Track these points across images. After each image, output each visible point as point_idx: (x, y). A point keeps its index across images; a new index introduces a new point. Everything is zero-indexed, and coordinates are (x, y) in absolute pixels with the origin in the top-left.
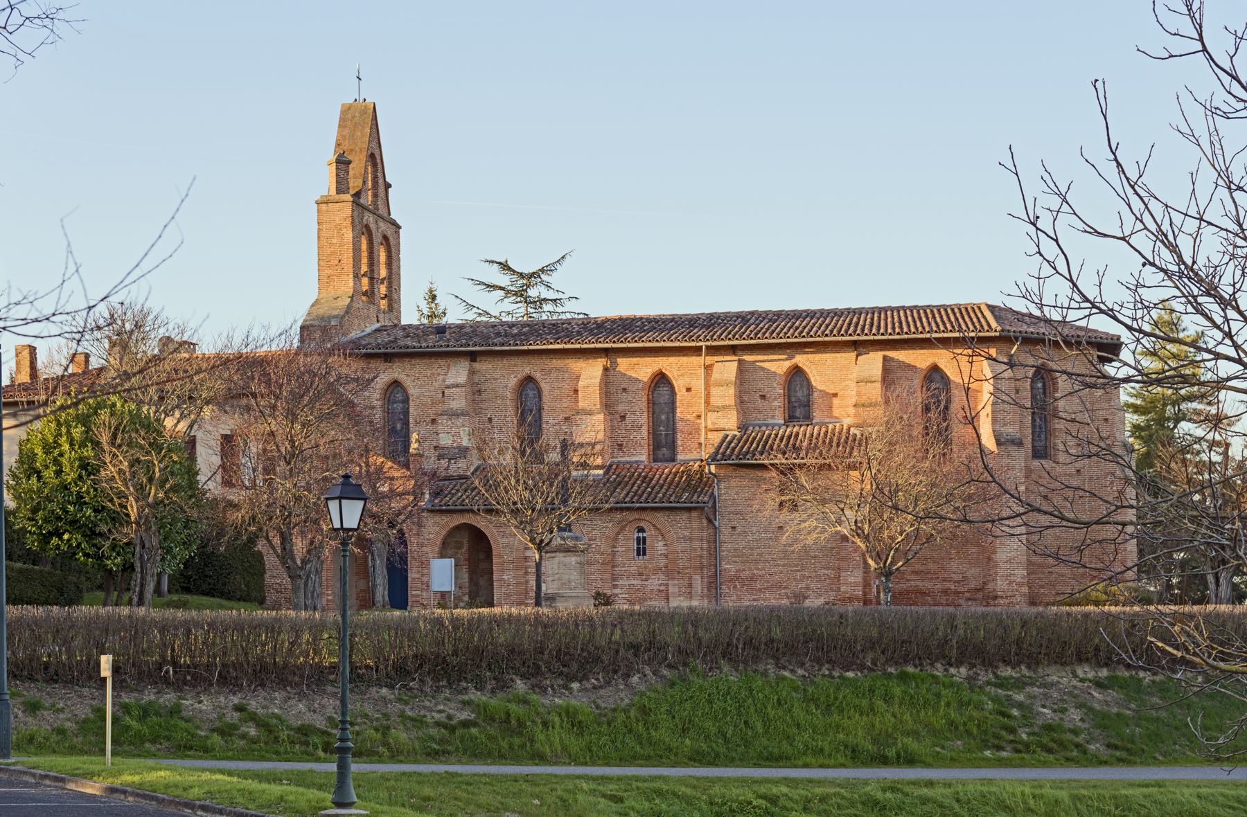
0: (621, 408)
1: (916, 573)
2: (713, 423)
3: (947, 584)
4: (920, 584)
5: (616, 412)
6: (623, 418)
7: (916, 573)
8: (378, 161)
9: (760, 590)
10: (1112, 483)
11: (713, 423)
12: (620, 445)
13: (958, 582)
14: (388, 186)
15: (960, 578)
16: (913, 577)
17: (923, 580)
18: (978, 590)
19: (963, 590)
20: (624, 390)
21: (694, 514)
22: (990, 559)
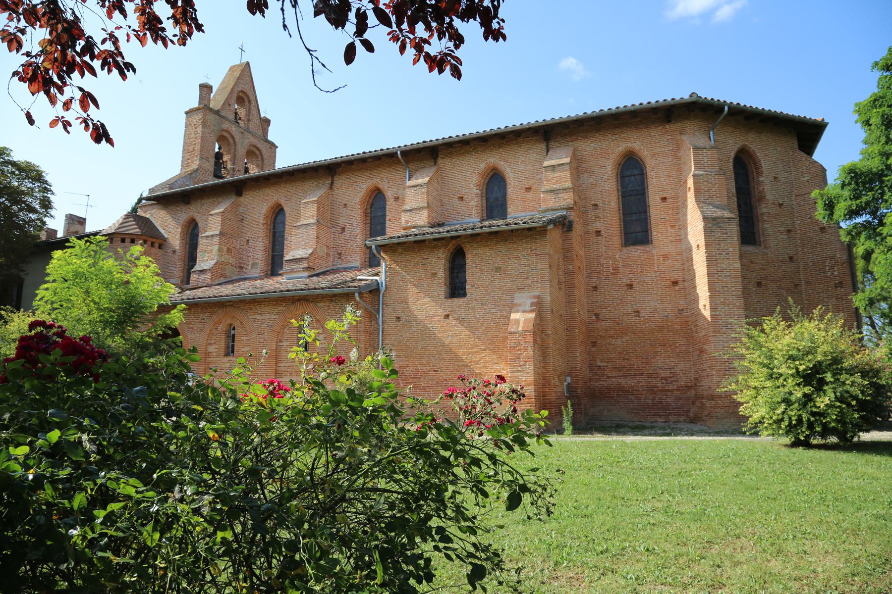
0: (342, 221)
1: (618, 369)
2: (407, 222)
3: (654, 382)
4: (623, 381)
5: (338, 225)
6: (343, 229)
7: (618, 369)
8: (252, 98)
9: (424, 389)
10: (832, 268)
11: (407, 222)
12: (340, 254)
13: (666, 379)
14: (266, 122)
15: (667, 374)
16: (614, 374)
17: (625, 377)
18: (689, 388)
19: (671, 387)
20: (345, 205)
21: (312, 287)
22: (702, 351)
